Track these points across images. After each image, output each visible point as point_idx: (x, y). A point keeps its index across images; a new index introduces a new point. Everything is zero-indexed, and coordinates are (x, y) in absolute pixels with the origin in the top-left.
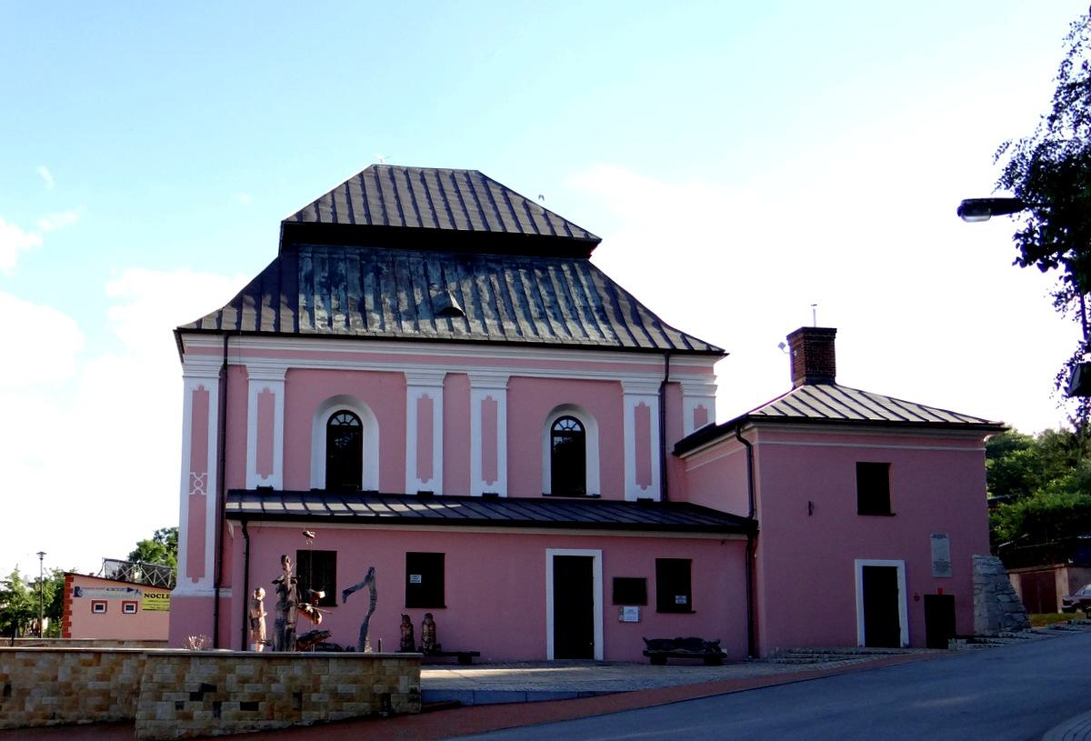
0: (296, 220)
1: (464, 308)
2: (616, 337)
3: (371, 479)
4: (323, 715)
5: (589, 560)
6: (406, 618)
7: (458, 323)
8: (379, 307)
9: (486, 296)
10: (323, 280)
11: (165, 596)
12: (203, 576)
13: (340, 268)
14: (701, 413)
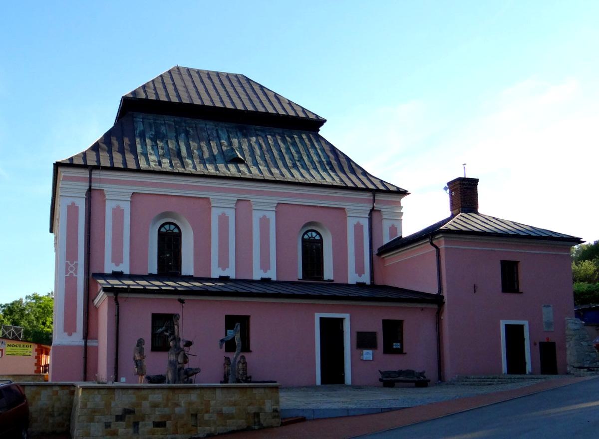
0: (131, 96)
1: (245, 158)
2: (342, 180)
3: (188, 267)
4: (213, 429)
5: (341, 321)
6: (227, 359)
7: (242, 168)
8: (190, 154)
9: (258, 152)
10: (152, 136)
11: (22, 346)
12: (75, 331)
13: (162, 129)
14: (395, 229)
